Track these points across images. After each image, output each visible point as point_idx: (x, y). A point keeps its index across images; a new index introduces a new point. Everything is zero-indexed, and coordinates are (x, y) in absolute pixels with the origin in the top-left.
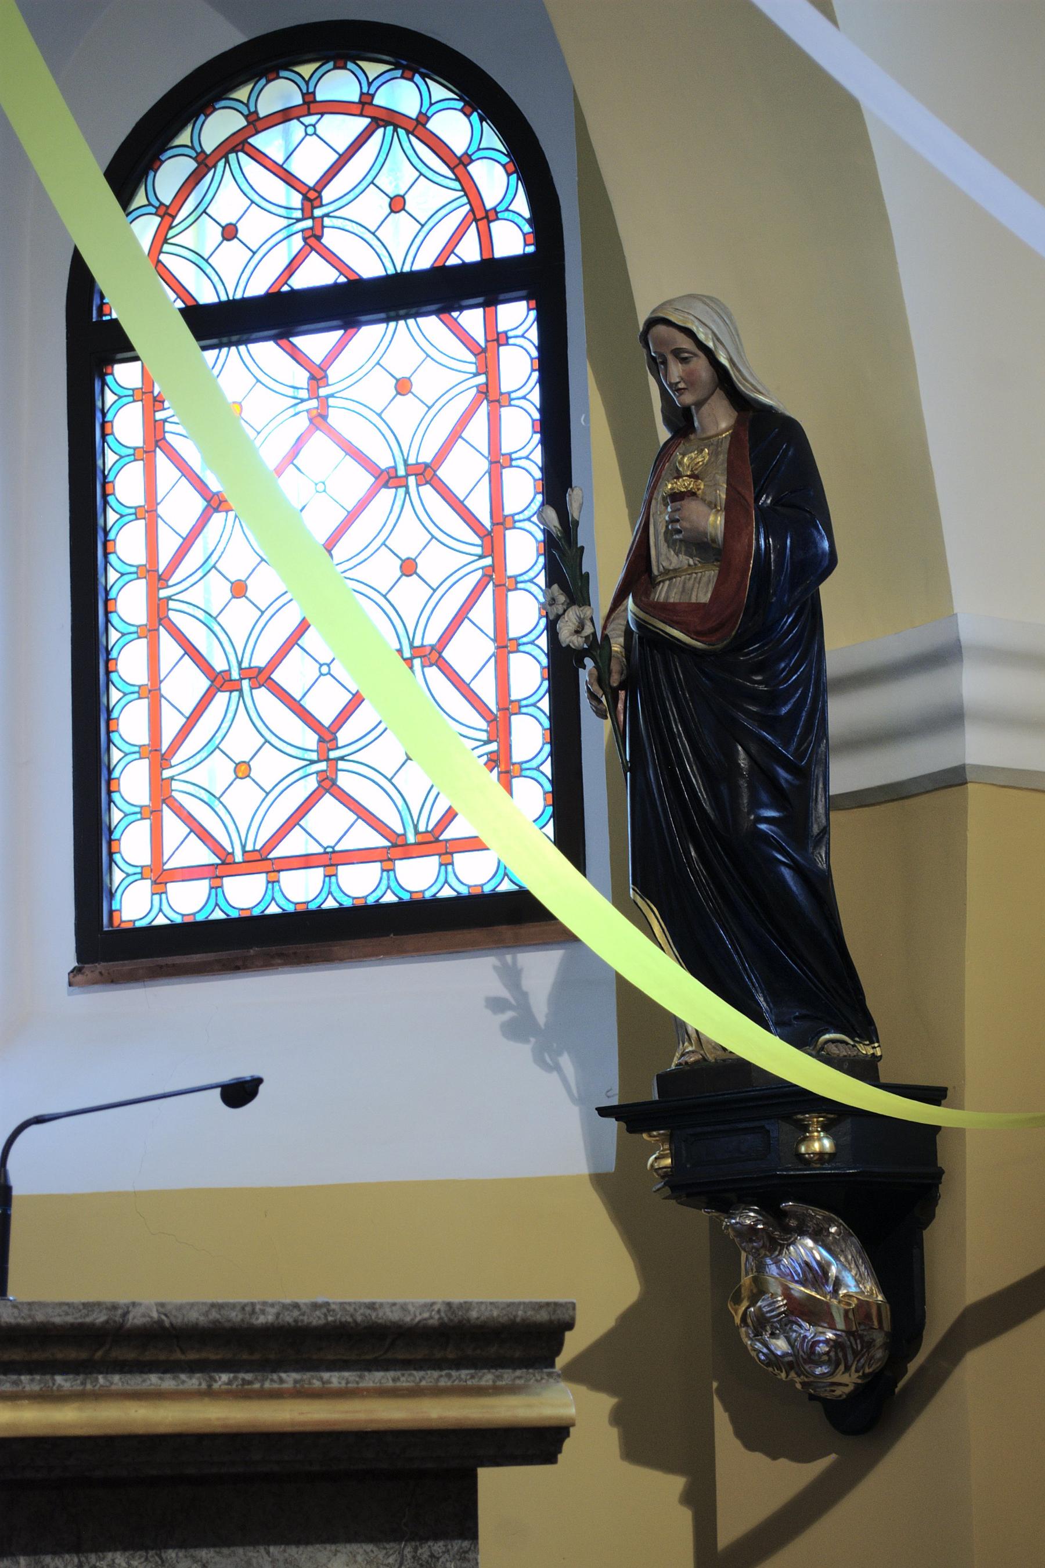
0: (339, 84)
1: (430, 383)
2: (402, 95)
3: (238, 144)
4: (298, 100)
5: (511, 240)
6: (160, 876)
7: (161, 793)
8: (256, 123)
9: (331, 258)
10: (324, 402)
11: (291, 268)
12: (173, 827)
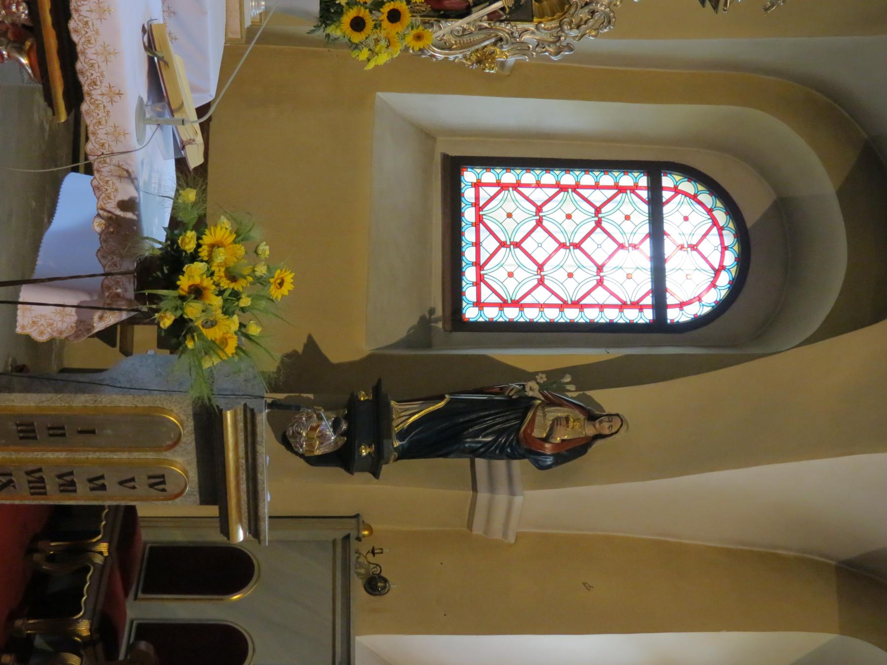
0: (730, 259)
1: (630, 285)
2: (724, 279)
3: (715, 223)
4: (726, 245)
5: (673, 315)
6: (477, 185)
7: (504, 187)
8: (720, 229)
9: (674, 252)
10: (568, 248)
11: (674, 242)
12: (493, 190)
